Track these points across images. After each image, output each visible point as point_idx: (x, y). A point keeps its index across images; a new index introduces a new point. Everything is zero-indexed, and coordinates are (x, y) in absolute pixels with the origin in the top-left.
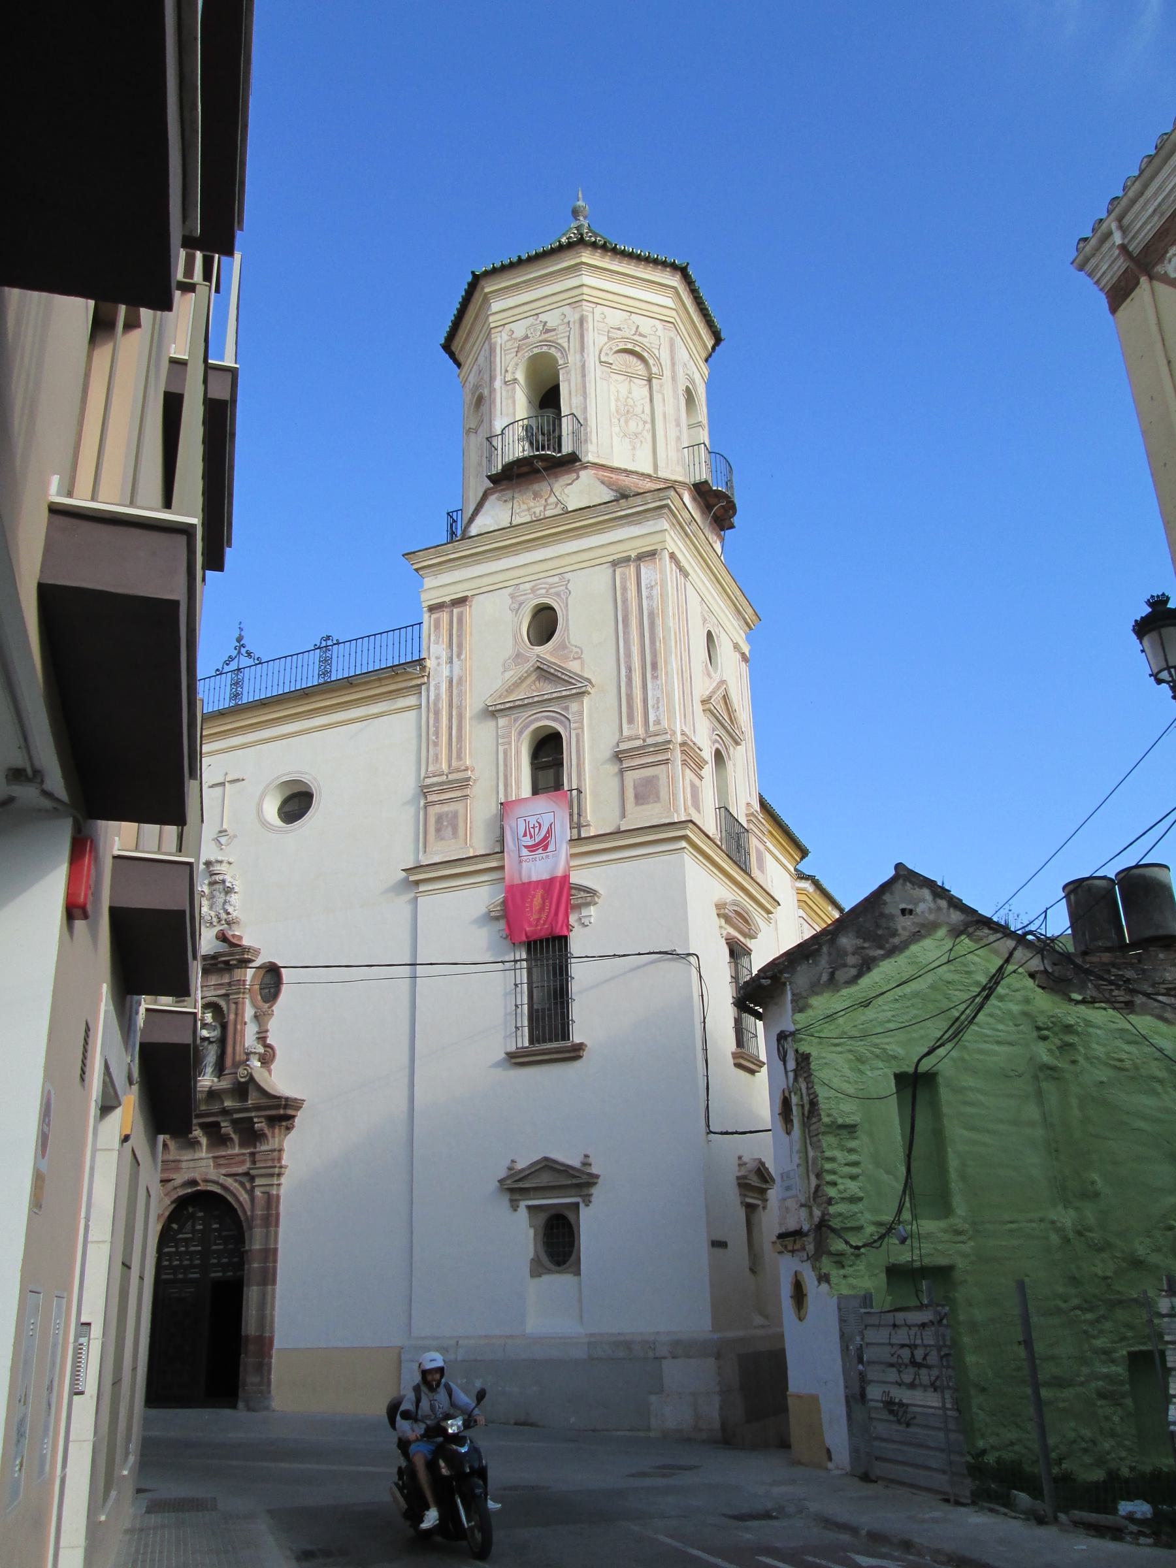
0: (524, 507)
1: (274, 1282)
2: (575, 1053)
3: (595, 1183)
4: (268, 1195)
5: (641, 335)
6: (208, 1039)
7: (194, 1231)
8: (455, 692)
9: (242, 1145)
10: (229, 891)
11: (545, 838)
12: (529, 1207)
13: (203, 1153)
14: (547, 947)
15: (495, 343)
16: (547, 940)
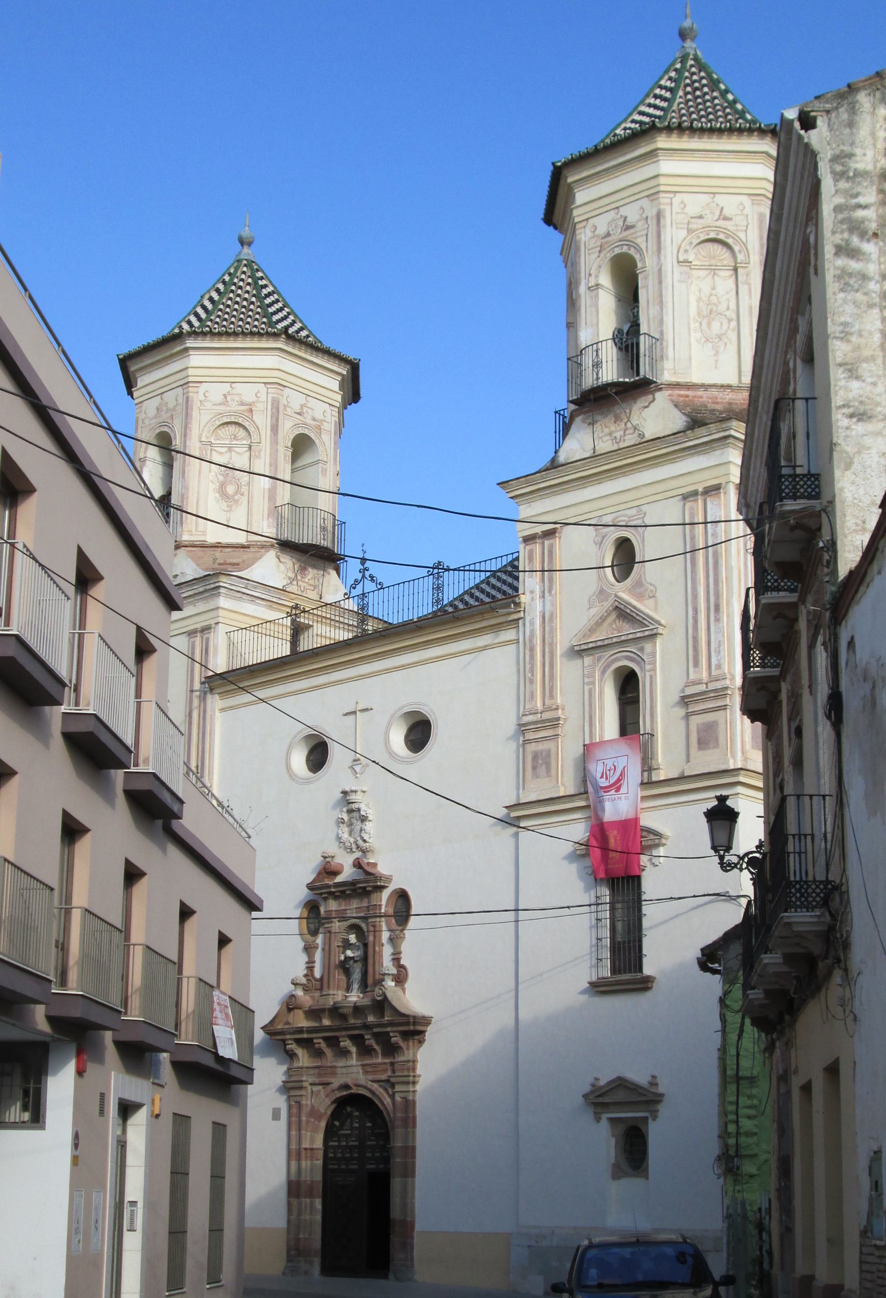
0: (606, 430)
1: (413, 1175)
2: (645, 984)
3: (660, 1101)
4: (405, 1099)
5: (726, 219)
6: (352, 958)
7: (352, 1128)
8: (547, 628)
9: (385, 1054)
10: (364, 819)
11: (619, 780)
12: (611, 1120)
13: (354, 1061)
14: (623, 883)
15: (580, 241)
16: (623, 878)
